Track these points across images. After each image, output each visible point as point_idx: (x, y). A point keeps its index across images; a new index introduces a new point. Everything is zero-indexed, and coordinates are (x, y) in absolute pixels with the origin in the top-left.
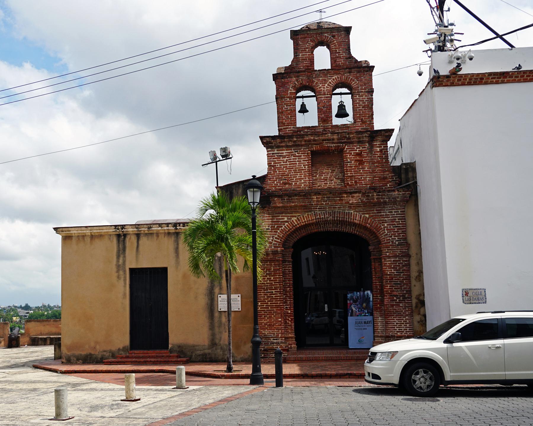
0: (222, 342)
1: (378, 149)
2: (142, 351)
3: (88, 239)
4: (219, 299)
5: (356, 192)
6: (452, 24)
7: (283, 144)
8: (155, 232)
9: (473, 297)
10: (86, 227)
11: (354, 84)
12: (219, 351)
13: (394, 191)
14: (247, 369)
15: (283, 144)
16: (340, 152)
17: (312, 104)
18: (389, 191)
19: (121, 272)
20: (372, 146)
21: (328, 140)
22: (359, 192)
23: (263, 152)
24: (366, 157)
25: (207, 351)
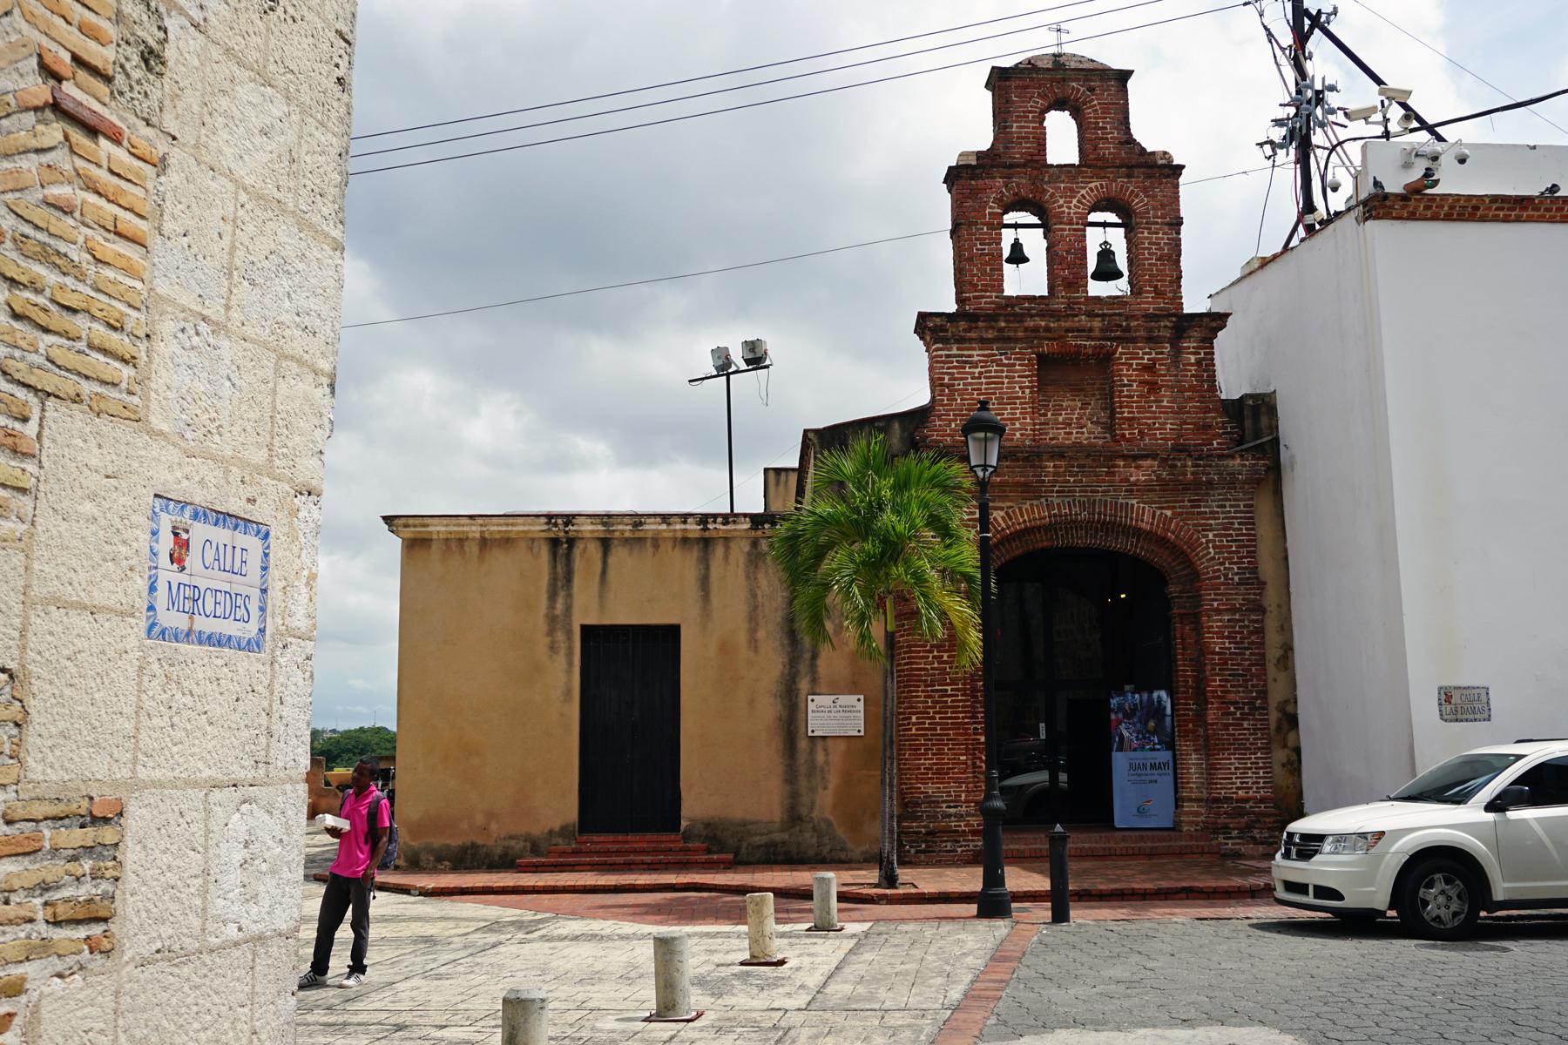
0: (815, 814)
1: (1193, 359)
2: (611, 838)
3: (474, 549)
4: (811, 706)
5: (1145, 457)
6: (1332, 88)
7: (973, 335)
8: (650, 535)
9: (1461, 705)
10: (471, 517)
11: (1139, 203)
12: (807, 835)
13: (1232, 457)
14: (971, 880)
15: (973, 335)
16: (1105, 360)
17: (1035, 243)
18: (1221, 457)
19: (560, 636)
20: (1178, 351)
21: (1078, 331)
22: (1154, 456)
23: (917, 354)
24: (1165, 375)
25: (777, 837)
